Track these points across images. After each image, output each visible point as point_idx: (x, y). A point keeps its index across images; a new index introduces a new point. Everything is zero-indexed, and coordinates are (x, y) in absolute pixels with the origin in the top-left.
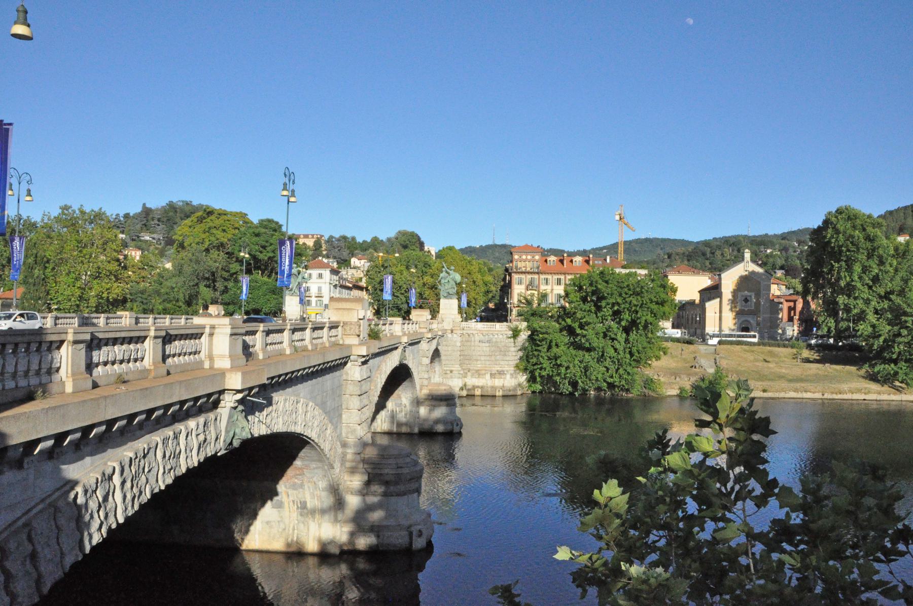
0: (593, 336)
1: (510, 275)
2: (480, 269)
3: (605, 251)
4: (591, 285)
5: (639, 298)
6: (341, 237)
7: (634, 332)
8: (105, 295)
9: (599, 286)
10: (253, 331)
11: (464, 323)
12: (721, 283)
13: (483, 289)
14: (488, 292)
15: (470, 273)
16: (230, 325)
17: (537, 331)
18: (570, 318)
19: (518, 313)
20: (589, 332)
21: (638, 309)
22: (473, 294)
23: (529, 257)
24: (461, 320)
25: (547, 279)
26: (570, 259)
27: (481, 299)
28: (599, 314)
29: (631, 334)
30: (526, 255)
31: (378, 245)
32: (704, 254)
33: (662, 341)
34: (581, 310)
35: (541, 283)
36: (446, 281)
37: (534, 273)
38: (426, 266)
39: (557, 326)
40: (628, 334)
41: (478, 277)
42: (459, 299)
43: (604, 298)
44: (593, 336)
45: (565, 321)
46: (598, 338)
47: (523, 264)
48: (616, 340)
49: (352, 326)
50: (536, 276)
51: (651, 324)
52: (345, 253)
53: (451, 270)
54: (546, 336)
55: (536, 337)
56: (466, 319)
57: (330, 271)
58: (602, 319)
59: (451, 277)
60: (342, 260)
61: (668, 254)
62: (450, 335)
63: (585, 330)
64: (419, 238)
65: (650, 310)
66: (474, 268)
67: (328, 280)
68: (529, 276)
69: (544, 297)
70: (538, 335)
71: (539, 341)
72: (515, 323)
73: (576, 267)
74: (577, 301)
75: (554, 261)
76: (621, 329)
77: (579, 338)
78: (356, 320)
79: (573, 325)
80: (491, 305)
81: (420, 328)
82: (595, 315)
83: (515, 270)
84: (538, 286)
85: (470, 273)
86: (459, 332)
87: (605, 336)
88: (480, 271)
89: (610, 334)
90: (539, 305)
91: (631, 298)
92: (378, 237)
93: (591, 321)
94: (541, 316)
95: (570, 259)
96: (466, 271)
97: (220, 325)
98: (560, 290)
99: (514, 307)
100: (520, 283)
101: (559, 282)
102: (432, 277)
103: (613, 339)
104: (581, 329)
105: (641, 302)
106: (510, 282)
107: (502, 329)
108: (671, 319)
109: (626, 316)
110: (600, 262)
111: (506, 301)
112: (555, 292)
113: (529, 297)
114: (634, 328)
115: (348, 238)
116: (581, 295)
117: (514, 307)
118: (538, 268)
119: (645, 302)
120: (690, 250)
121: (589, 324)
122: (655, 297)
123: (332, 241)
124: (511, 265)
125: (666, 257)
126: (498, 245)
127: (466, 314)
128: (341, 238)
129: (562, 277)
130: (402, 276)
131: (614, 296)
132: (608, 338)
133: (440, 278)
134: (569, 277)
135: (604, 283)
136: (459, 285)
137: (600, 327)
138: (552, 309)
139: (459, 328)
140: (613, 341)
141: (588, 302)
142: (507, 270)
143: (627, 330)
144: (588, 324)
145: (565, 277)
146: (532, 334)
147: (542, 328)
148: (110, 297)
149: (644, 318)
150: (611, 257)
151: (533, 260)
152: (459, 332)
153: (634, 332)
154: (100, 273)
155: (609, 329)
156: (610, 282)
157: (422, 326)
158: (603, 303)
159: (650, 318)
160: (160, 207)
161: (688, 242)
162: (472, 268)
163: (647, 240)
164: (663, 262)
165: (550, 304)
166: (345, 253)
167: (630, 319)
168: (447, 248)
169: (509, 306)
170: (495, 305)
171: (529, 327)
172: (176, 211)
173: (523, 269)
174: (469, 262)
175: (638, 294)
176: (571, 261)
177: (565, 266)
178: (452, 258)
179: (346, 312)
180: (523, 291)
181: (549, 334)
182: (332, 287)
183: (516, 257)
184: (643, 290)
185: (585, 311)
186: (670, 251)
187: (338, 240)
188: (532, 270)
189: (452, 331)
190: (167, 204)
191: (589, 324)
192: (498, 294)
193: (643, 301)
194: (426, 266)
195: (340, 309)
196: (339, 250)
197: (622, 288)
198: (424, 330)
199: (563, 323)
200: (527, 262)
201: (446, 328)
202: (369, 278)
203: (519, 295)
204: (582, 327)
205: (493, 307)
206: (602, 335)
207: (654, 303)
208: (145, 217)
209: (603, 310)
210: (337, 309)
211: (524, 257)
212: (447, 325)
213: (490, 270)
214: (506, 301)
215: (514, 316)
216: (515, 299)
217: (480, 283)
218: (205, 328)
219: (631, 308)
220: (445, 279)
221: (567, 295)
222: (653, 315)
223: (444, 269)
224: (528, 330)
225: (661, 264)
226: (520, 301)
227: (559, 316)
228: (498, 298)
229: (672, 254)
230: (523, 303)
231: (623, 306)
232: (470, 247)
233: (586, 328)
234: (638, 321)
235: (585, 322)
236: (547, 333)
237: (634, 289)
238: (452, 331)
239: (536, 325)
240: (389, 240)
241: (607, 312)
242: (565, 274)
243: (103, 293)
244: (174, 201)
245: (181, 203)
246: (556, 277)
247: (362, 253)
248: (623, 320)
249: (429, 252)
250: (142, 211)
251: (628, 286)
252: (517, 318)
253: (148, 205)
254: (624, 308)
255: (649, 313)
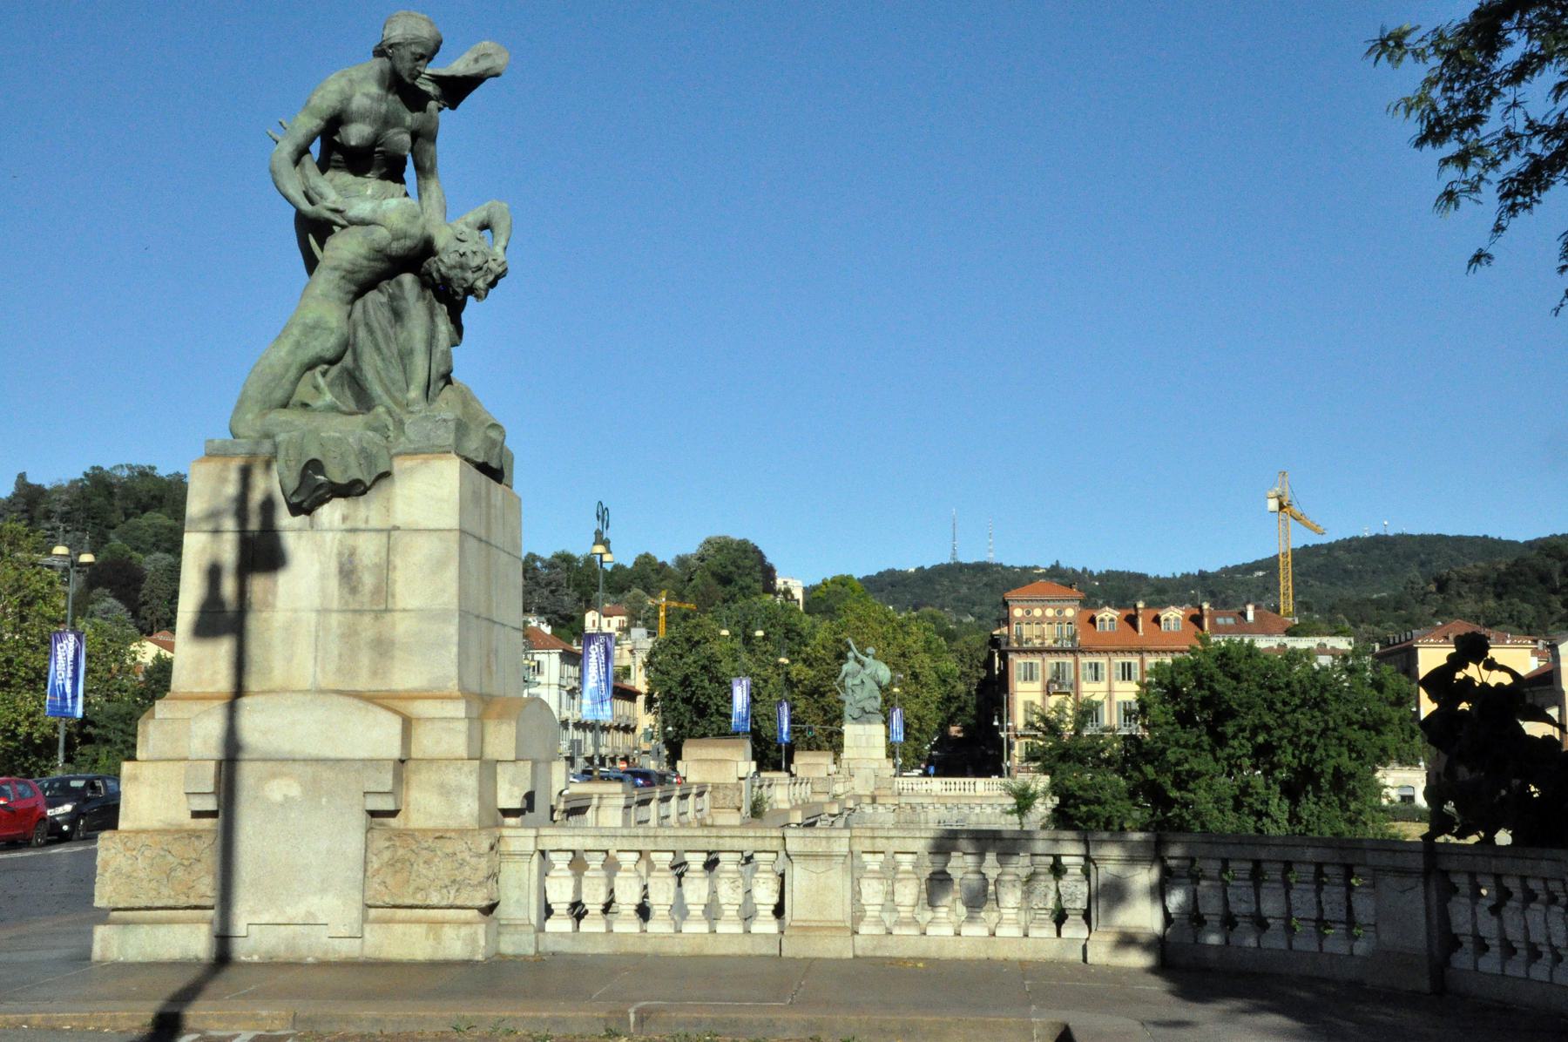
0: (1210, 805)
1: (1004, 657)
2: (928, 642)
3: (1261, 574)
4: (1200, 686)
5: (1317, 713)
6: (557, 556)
7: (1310, 796)
8: (22, 730)
9: (1217, 687)
10: (581, 808)
11: (898, 779)
12: (1559, 669)
13: (938, 693)
14: (948, 699)
15: (903, 655)
16: (623, 793)
17: (1073, 796)
18: (1151, 762)
19: (1027, 753)
20: (1202, 797)
21: (1314, 740)
22: (915, 707)
23: (1050, 612)
24: (893, 771)
25: (1096, 665)
26: (1152, 613)
27: (933, 718)
28: (1219, 753)
29: (1304, 801)
30: (1043, 609)
31: (654, 577)
32: (1544, 578)
33: (1388, 820)
34: (1177, 743)
35: (1081, 678)
36: (857, 682)
37: (1064, 651)
38: (790, 635)
39: (1123, 782)
40: (1295, 802)
41: (923, 662)
42: (887, 722)
43: (1231, 714)
44: (1210, 805)
45: (1141, 771)
46: (1222, 812)
47: (1036, 630)
48: (1267, 815)
49: (728, 792)
50: (1069, 660)
51: (1352, 776)
52: (568, 599)
53: (867, 655)
54: (1096, 808)
55: (1072, 811)
56: (901, 770)
57: (561, 654)
58: (1229, 765)
59: (868, 671)
60: (561, 617)
61: (1436, 580)
62: (869, 810)
63: (1190, 791)
64: (761, 557)
65: (1345, 742)
66: (915, 641)
67: (555, 679)
68: (1052, 660)
69: (1087, 712)
70: (1076, 807)
71: (1080, 819)
72: (1022, 778)
73: (1169, 633)
74: (1167, 723)
75: (1112, 620)
76: (1277, 788)
77: (1176, 810)
78: (735, 781)
79: (1160, 780)
80: (954, 730)
81: (813, 792)
82: (1210, 757)
83: (1016, 645)
84: (1075, 685)
85: (903, 655)
86: (891, 801)
87: (1238, 806)
88: (927, 650)
89: (1251, 800)
90: (1078, 733)
91: (1298, 715)
92: (652, 553)
93: (1202, 768)
94: (1082, 761)
95: (1152, 613)
96: (896, 651)
97: (608, 794)
98: (1128, 692)
99: (1016, 736)
100: (1030, 676)
101: (1126, 672)
102: (810, 666)
103: (1260, 815)
104: (1179, 789)
105: (1322, 725)
106: (1005, 673)
107: (991, 793)
108: (1422, 764)
109: (1286, 756)
110: (1230, 621)
111: (996, 723)
112: (1119, 697)
113: (1053, 716)
114: (1310, 788)
115: (577, 560)
116: (1177, 708)
117: (1016, 736)
118: (1073, 638)
119: (1331, 724)
120: (1502, 567)
121: (1199, 775)
122: (1357, 711)
123: (535, 569)
124: (1005, 630)
125: (1433, 588)
126: (967, 566)
127: (905, 756)
128: (557, 561)
129: (1134, 660)
130: (737, 665)
131: (1257, 711)
132: (1246, 810)
133: (843, 674)
134: (1151, 660)
135: (1228, 680)
136: (884, 690)
137: (1224, 784)
138: (1109, 744)
139: (889, 792)
140: (1260, 819)
141: (1195, 724)
142: (994, 642)
143: (1291, 792)
144: (1195, 775)
145: (1142, 661)
146: (1063, 804)
147: (1086, 790)
148: (36, 735)
149: (1332, 763)
150: (1256, 608)
151: (1059, 620)
152: (891, 801)
153: (1310, 796)
154: (11, 675)
155: (1245, 789)
156: (1245, 676)
157: (818, 789)
158: (1230, 728)
159: (1347, 764)
160: (66, 485)
161: (1499, 542)
162: (909, 641)
163: (1378, 541)
164: (1423, 602)
165: (1105, 730)
166: (568, 599)
167: (1295, 763)
168: (833, 581)
169: (1003, 735)
170: (965, 728)
171: (1054, 789)
172: (111, 494)
173: (1037, 642)
174: (902, 626)
175: (1316, 705)
176: (1157, 620)
177: (1141, 633)
178: (859, 619)
179: (716, 766)
180: (1037, 699)
181: (1105, 802)
182: (564, 694)
183: (1018, 612)
184: (1327, 695)
185: (1186, 746)
186: (1444, 571)
187: (550, 565)
188: (1058, 645)
189: (874, 799)
190: (86, 474)
191: (1199, 775)
192: (972, 701)
193: (1326, 722)
194: (790, 635)
195: (706, 760)
196: (552, 592)
197: (1272, 689)
198: (824, 798)
199: (1136, 774)
200: (1045, 626)
201: (861, 792)
202: (657, 670)
203: (1030, 707)
204: (1180, 784)
205: (961, 735)
206: (1230, 803)
207: (1356, 727)
208: (23, 511)
209: (1231, 742)
210: (698, 760)
211: (1037, 612)
212: (862, 786)
213: (950, 636)
214: (996, 723)
215: (1017, 760)
216: (1019, 719)
217: (930, 677)
218: (591, 798)
219: (1299, 738)
220: (854, 677)
221: (1144, 707)
222: (1354, 755)
223: (850, 654)
224: (1054, 794)
225: (1417, 609)
226: (1030, 725)
227: (1125, 760)
228: (971, 710)
229: (1449, 579)
230: (1038, 729)
231: (1277, 733)
232: (891, 572)
233: (1192, 785)
234: (1317, 770)
235: (1189, 772)
236: (1098, 801)
237: (1304, 692)
238: (874, 799)
239: (1070, 783)
240: (682, 561)
241: (1240, 746)
242: (1140, 652)
243: (18, 724)
244: (106, 468)
245: (126, 473)
246: (1119, 660)
247: (612, 598)
248: (1279, 766)
249: (787, 592)
250: (15, 495)
251: (1288, 685)
252: (1025, 765)
253: (32, 479)
254: (1281, 739)
255: (1344, 750)
